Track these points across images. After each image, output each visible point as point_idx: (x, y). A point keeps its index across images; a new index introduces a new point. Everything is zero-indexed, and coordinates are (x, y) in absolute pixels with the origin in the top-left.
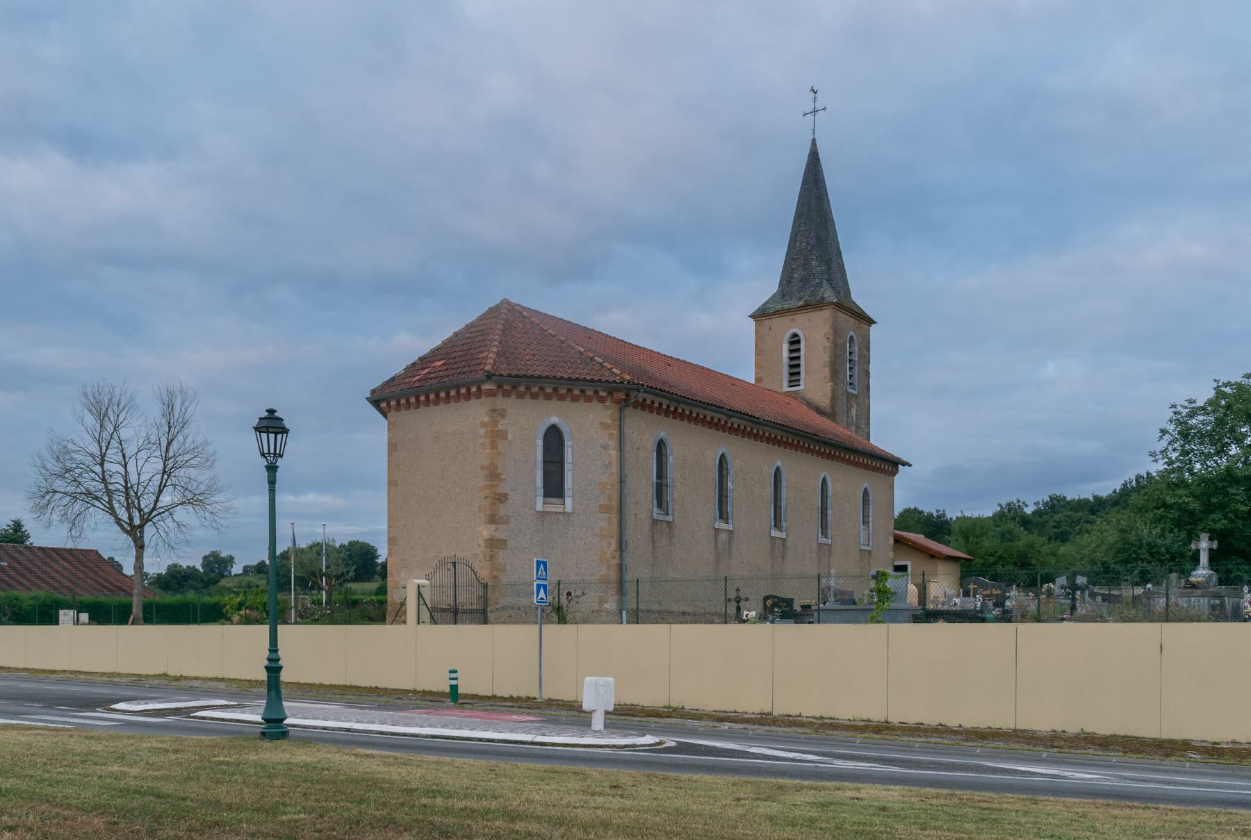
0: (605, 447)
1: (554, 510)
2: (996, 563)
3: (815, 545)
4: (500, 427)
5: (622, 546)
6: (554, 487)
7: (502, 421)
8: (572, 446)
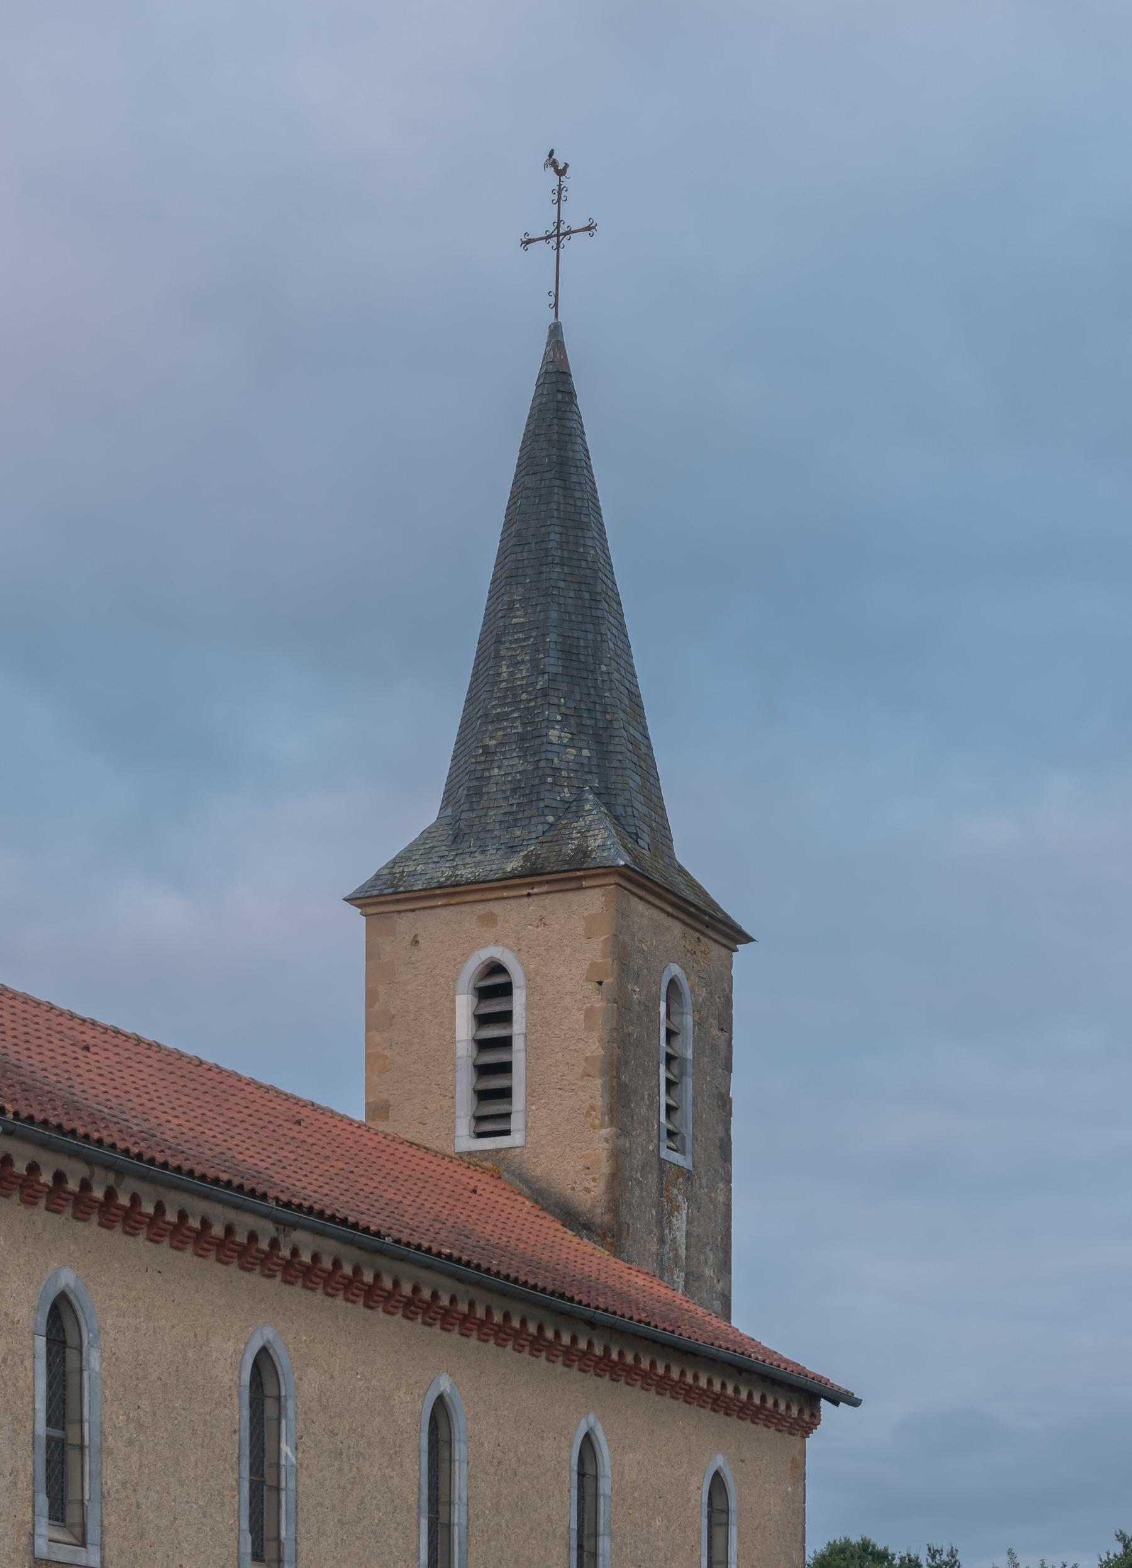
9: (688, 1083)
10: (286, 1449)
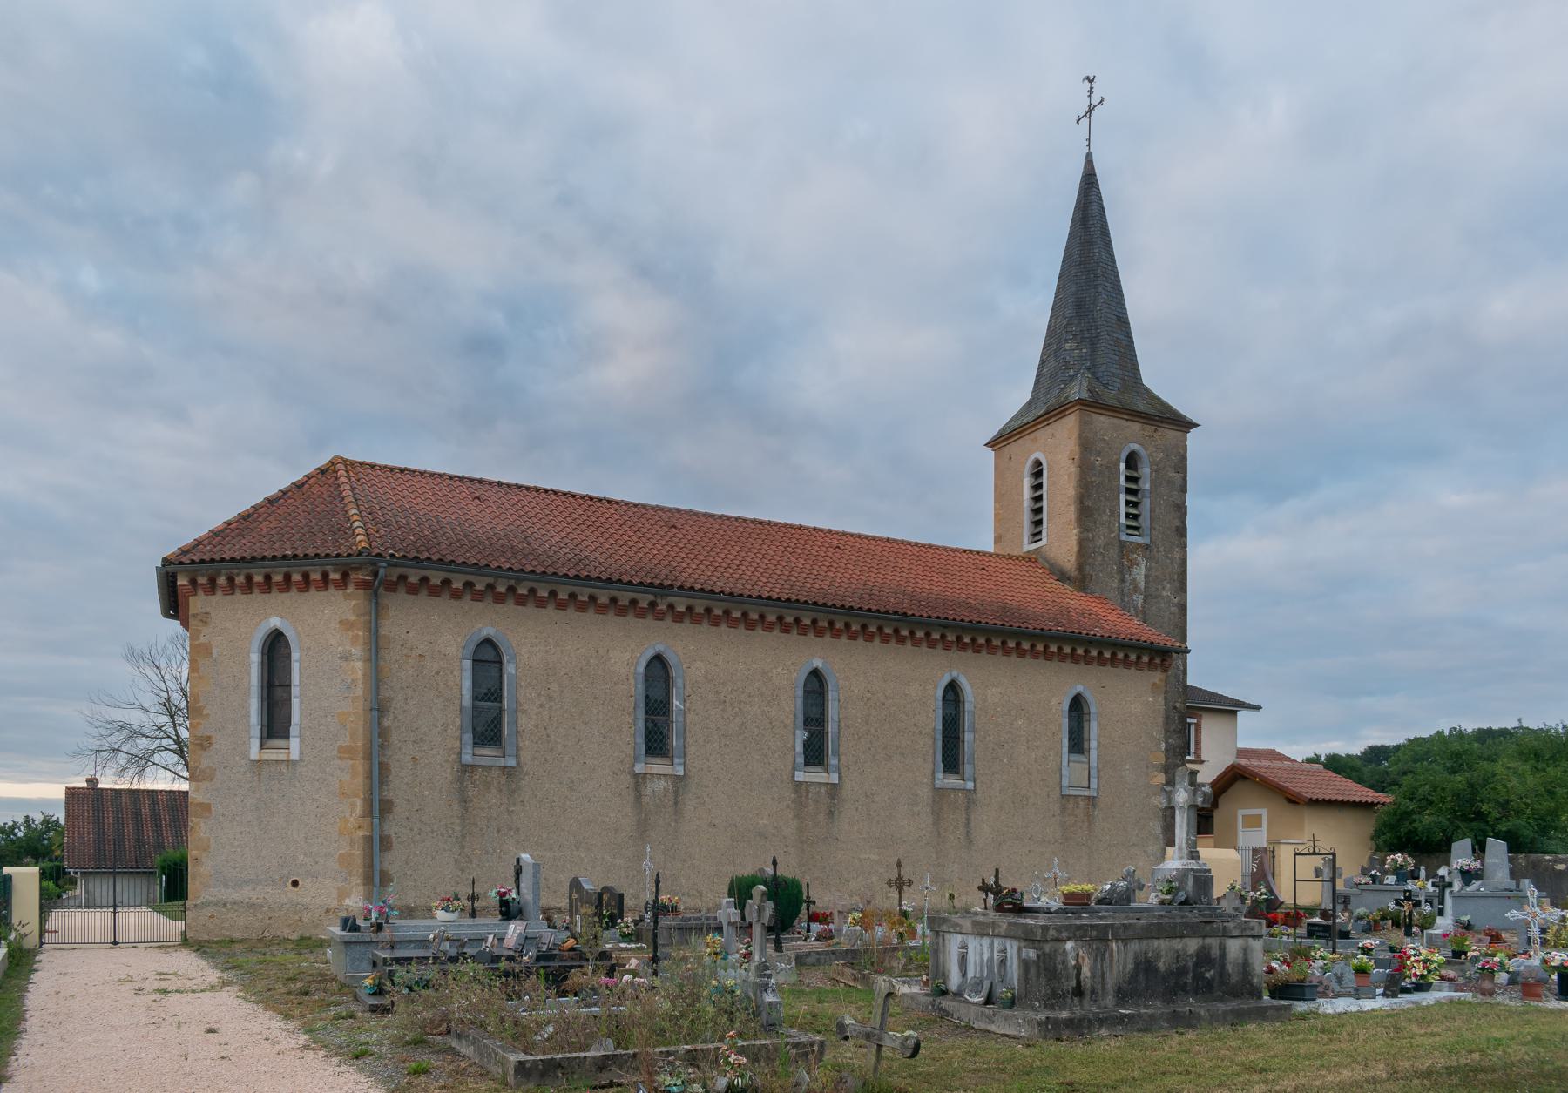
0: (346, 657)
1: (274, 757)
2: (1421, 811)
3: (925, 793)
4: (202, 640)
5: (379, 807)
6: (275, 725)
7: (205, 630)
8: (300, 661)
9: (1146, 504)
10: (676, 702)
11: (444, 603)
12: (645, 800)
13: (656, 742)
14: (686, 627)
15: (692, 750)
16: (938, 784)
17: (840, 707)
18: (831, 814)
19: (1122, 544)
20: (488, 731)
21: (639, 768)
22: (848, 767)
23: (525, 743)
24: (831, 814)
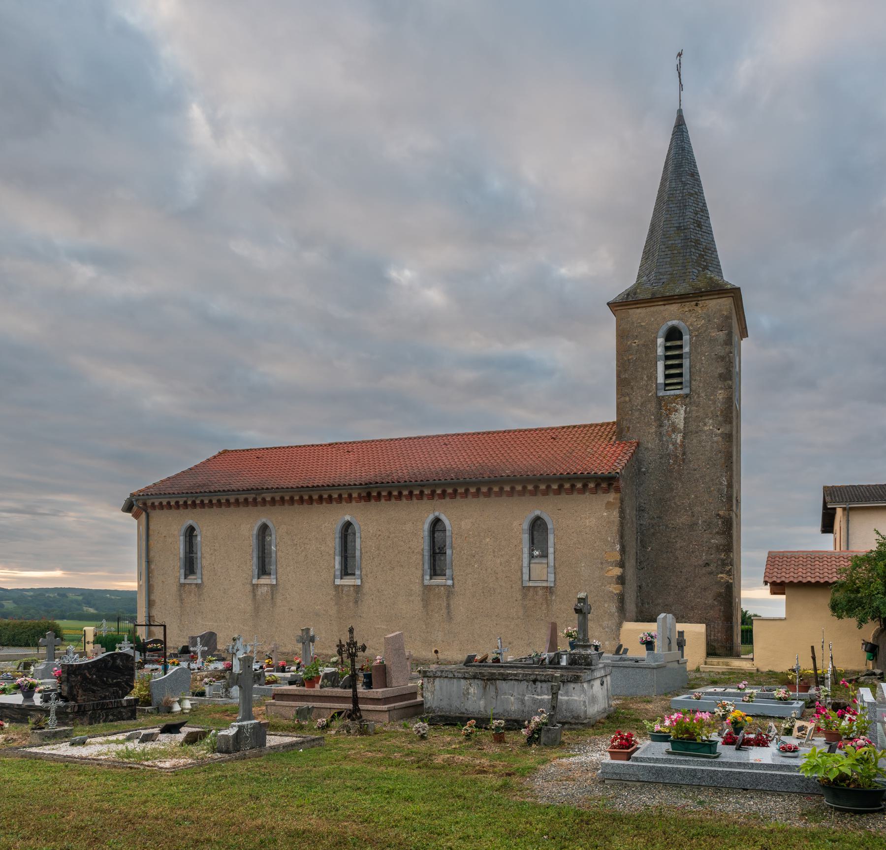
3: (417, 588)
11: (243, 510)
12: (258, 597)
13: (263, 570)
14: (277, 508)
15: (280, 571)
16: (426, 582)
17: (361, 542)
18: (356, 602)
19: (660, 400)
20: (190, 566)
21: (255, 581)
22: (367, 575)
23: (205, 572)
24: (356, 602)
